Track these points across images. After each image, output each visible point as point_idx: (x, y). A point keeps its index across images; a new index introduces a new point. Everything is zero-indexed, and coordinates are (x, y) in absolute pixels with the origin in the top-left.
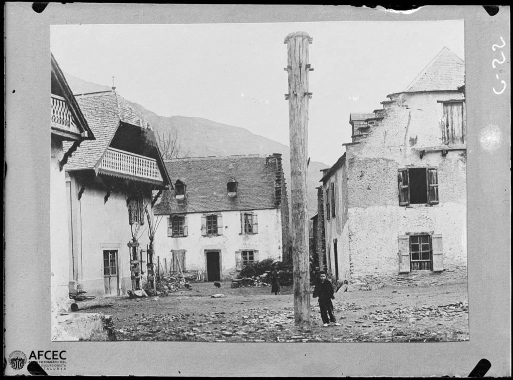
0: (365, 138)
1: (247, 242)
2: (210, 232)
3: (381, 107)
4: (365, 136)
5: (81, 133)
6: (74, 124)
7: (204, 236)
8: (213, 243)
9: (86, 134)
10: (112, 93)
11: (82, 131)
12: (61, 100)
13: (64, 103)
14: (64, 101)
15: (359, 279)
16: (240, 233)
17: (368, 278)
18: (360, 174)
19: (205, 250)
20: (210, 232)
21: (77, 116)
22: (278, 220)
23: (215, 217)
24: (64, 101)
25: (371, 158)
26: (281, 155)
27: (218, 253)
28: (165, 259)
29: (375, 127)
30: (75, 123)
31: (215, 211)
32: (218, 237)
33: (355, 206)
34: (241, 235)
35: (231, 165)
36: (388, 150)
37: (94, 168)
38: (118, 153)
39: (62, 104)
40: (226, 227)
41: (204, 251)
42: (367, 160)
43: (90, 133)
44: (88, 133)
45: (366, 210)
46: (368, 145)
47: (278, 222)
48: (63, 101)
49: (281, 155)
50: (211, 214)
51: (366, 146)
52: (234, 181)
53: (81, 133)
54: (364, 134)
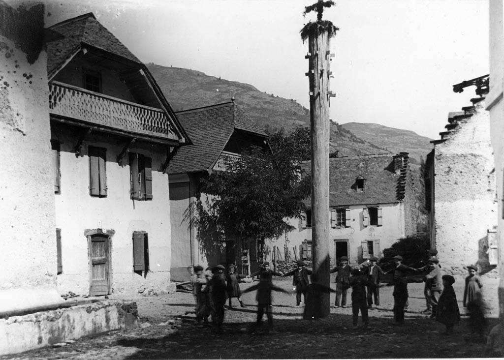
0: (453, 135)
1: (373, 233)
2: (339, 224)
3: (471, 104)
4: (452, 133)
5: (179, 139)
6: (172, 132)
7: (334, 228)
8: (342, 234)
9: (183, 140)
10: (232, 104)
11: (180, 138)
12: (159, 112)
13: (162, 114)
14: (162, 113)
15: (444, 270)
16: (490, 231)
17: (453, 269)
18: (447, 170)
19: (335, 240)
20: (339, 224)
21: (175, 125)
22: (401, 213)
23: (344, 211)
24: (162, 113)
25: (459, 154)
26: (408, 154)
27: (346, 243)
28: (58, 232)
29: (464, 124)
30: (173, 131)
31: (343, 206)
32: (347, 228)
33: (442, 201)
34: (487, 232)
35: (361, 164)
36: (476, 146)
37: (207, 170)
38: (232, 156)
39: (157, 114)
40: (354, 220)
41: (333, 241)
42: (454, 157)
43: (187, 138)
44: (186, 139)
45: (452, 204)
46: (456, 141)
47: (401, 215)
48: (161, 112)
49: (408, 154)
50: (340, 207)
51: (454, 143)
52: (362, 178)
53: (179, 139)
54: (453, 131)
